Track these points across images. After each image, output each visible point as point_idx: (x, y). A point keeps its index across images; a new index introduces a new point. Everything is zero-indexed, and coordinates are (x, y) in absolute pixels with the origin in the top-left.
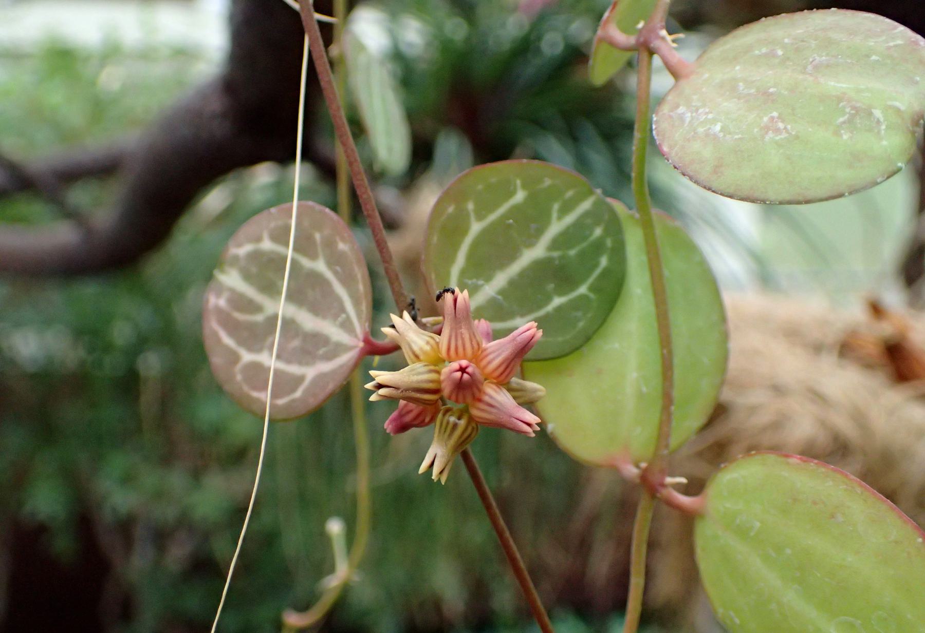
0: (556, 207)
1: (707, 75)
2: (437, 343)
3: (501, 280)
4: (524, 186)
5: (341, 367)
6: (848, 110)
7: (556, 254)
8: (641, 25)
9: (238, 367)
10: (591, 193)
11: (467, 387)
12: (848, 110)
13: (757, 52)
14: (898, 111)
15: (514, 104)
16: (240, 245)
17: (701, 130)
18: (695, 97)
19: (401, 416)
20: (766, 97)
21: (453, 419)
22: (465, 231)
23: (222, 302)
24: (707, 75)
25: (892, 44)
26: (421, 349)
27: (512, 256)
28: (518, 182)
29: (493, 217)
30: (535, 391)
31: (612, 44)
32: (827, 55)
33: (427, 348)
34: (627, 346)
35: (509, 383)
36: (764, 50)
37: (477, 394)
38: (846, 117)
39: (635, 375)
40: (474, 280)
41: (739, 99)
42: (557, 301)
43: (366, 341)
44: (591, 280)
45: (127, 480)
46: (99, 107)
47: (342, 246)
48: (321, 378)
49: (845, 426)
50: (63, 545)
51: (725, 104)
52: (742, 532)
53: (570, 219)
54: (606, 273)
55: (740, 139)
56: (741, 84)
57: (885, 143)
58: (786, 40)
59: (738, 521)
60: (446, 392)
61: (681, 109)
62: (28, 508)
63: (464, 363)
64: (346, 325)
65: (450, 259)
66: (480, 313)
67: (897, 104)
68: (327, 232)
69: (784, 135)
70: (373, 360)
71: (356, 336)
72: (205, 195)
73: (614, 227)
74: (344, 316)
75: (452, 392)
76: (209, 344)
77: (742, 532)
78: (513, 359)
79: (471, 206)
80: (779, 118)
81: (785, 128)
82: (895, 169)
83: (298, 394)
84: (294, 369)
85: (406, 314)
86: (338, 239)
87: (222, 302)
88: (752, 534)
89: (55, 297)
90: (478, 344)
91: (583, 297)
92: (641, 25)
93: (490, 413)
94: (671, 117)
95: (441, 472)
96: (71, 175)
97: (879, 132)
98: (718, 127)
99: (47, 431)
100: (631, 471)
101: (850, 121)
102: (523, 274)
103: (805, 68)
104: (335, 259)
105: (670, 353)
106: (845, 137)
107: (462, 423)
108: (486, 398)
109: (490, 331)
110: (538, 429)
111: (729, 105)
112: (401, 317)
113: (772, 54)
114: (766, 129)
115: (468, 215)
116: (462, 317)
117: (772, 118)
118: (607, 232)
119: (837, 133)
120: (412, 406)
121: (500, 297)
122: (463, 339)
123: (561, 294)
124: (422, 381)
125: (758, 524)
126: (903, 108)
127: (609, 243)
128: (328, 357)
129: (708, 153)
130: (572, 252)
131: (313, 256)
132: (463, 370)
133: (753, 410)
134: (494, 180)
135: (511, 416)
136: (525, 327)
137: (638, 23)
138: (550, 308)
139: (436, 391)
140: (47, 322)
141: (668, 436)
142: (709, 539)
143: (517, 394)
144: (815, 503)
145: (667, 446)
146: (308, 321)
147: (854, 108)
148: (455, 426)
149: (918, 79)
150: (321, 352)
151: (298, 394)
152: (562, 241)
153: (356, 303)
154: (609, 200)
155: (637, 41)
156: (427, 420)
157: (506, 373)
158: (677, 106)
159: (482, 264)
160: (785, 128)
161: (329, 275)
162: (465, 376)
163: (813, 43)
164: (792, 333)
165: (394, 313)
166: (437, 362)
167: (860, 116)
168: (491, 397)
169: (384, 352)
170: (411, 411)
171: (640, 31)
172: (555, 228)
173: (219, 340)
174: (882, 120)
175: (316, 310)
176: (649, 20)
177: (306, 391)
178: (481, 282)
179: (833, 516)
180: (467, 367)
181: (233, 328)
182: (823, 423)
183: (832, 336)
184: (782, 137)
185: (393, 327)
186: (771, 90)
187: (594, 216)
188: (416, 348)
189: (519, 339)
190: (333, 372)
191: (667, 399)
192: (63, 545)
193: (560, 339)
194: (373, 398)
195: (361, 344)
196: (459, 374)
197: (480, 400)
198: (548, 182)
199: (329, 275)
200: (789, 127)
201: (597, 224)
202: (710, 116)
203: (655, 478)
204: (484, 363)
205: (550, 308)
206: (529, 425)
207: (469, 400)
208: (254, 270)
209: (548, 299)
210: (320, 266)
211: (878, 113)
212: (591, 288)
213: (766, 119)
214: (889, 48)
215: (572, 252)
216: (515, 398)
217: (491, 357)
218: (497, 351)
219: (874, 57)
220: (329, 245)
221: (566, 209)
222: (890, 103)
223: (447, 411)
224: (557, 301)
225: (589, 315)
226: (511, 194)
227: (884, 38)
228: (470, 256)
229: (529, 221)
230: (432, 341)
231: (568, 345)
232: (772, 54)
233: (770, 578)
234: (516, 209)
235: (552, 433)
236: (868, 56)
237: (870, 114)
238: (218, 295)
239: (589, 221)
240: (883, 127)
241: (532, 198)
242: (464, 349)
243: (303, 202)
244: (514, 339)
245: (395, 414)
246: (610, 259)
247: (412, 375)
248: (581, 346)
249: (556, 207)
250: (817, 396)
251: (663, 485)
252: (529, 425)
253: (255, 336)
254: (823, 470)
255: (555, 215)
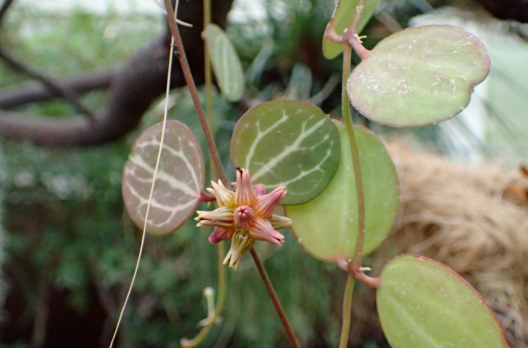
0: (304, 124)
1: (375, 58)
2: (233, 196)
3: (273, 162)
4: (287, 113)
5: (189, 207)
6: (438, 79)
7: (303, 149)
8: (345, 31)
9: (139, 206)
10: (324, 117)
11: (247, 220)
12: (438, 79)
13: (400, 47)
14: (462, 80)
15: (307, 62)
16: (141, 142)
17: (368, 87)
18: (368, 70)
19: (216, 234)
20: (401, 72)
21: (241, 236)
22: (254, 138)
23: (132, 172)
24: (375, 58)
25: (465, 44)
26: (225, 200)
27: (280, 150)
28: (284, 111)
29: (269, 130)
30: (286, 221)
31: (332, 40)
32: (433, 50)
33: (228, 199)
34: (342, 197)
35: (271, 217)
36: (403, 46)
37: (252, 223)
38: (438, 82)
39: (346, 213)
40: (259, 163)
41: (388, 72)
42: (303, 174)
43: (202, 194)
44: (321, 163)
45: (116, 264)
46: (104, 48)
47: (191, 144)
48: (179, 213)
49: (503, 237)
50: (79, 301)
51: (381, 74)
52: (397, 297)
53: (312, 130)
54: (329, 159)
55: (386, 93)
56: (390, 64)
57: (455, 97)
58: (414, 41)
59: (395, 291)
60: (236, 221)
61: (361, 76)
62: (59, 280)
63: (243, 207)
64: (193, 186)
65: (246, 152)
66: (260, 180)
67: (462, 76)
68: (184, 136)
69: (407, 92)
70: (207, 204)
71: (197, 191)
72: (159, 103)
73: (336, 135)
74: (191, 181)
75: (238, 222)
76: (125, 194)
77: (397, 297)
78: (271, 205)
79: (258, 124)
80: (405, 82)
81: (407, 88)
82: (459, 110)
83: (168, 221)
84: (167, 208)
85: (220, 181)
86: (189, 140)
87: (132, 172)
88: (402, 298)
89: (78, 158)
90: (254, 197)
91: (317, 172)
92: (345, 31)
93: (258, 233)
94: (356, 80)
95: (235, 264)
96: (84, 89)
97: (452, 91)
98: (376, 87)
99: (71, 235)
100: (343, 264)
101: (439, 85)
102: (285, 159)
103: (421, 56)
104: (188, 151)
105: (363, 201)
106: (436, 93)
107: (245, 238)
108: (257, 225)
109: (264, 190)
110: (283, 241)
111: (383, 75)
112: (217, 182)
113: (406, 49)
114: (398, 88)
115: (256, 128)
116: (246, 184)
117: (402, 82)
118: (331, 137)
119: (432, 91)
120: (220, 229)
121: (272, 172)
122: (245, 195)
123: (305, 170)
124: (223, 217)
125: (404, 293)
126: (465, 79)
127: (332, 143)
128: (184, 202)
129: (370, 100)
130: (312, 148)
131: (177, 149)
132: (242, 211)
133: (453, 228)
134: (270, 110)
135: (269, 235)
136: (281, 188)
137: (344, 29)
138: (299, 177)
139: (231, 222)
140: (73, 172)
141: (362, 245)
142: (383, 300)
143: (275, 223)
144: (431, 281)
145: (361, 251)
146: (174, 183)
147: (441, 78)
148: (241, 240)
149: (475, 63)
150: (180, 199)
151: (168, 221)
152: (306, 142)
153: (198, 175)
154: (333, 120)
155: (343, 39)
156: (228, 236)
157: (269, 212)
158: (360, 74)
159: (263, 154)
160: (407, 88)
161: (185, 159)
162: (244, 214)
163: (427, 43)
164: (478, 184)
165: (214, 181)
166: (233, 207)
167: (444, 82)
168: (259, 224)
169: (208, 201)
170: (219, 232)
171: (345, 33)
172: (304, 135)
173: (130, 192)
174: (454, 85)
175: (179, 177)
176: (349, 28)
177: (172, 219)
178: (262, 164)
179: (439, 289)
180: (244, 210)
181: (138, 186)
182: (491, 236)
183: (500, 187)
184: (406, 92)
185: (212, 188)
186: (404, 68)
187: (324, 129)
188: (223, 199)
189: (274, 195)
190: (186, 210)
191: (362, 226)
192: (79, 301)
193: (304, 194)
194: (198, 225)
195: (199, 196)
196: (240, 213)
197: (254, 226)
198: (300, 111)
199: (185, 159)
200: (409, 87)
201: (326, 133)
202: (374, 80)
203: (355, 268)
204: (257, 207)
205: (299, 177)
206: (279, 240)
207: (248, 226)
208: (148, 155)
209: (298, 173)
210: (181, 154)
211: (453, 81)
212: (322, 167)
213: (399, 83)
214: (463, 47)
215: (312, 148)
216: (273, 225)
217: (260, 204)
218: (264, 201)
219: (455, 52)
220: (185, 143)
221: (308, 126)
222: (459, 76)
223: (238, 232)
224: (303, 174)
225: (321, 181)
226: (281, 117)
227: (462, 41)
228: (257, 150)
229: (289, 132)
230: (231, 196)
231: (308, 197)
232: (406, 49)
233: (410, 321)
234: (283, 124)
235: (301, 243)
236: (452, 51)
237: (449, 82)
238: (130, 169)
239: (322, 131)
240: (455, 89)
241: (291, 119)
242: (246, 200)
243: (169, 121)
244: (272, 195)
245: (213, 233)
246: (332, 152)
247: (220, 213)
248: (315, 197)
249: (304, 124)
250: (489, 221)
251: (359, 271)
252: (279, 240)
253: (145, 190)
254: (435, 264)
255: (303, 128)
